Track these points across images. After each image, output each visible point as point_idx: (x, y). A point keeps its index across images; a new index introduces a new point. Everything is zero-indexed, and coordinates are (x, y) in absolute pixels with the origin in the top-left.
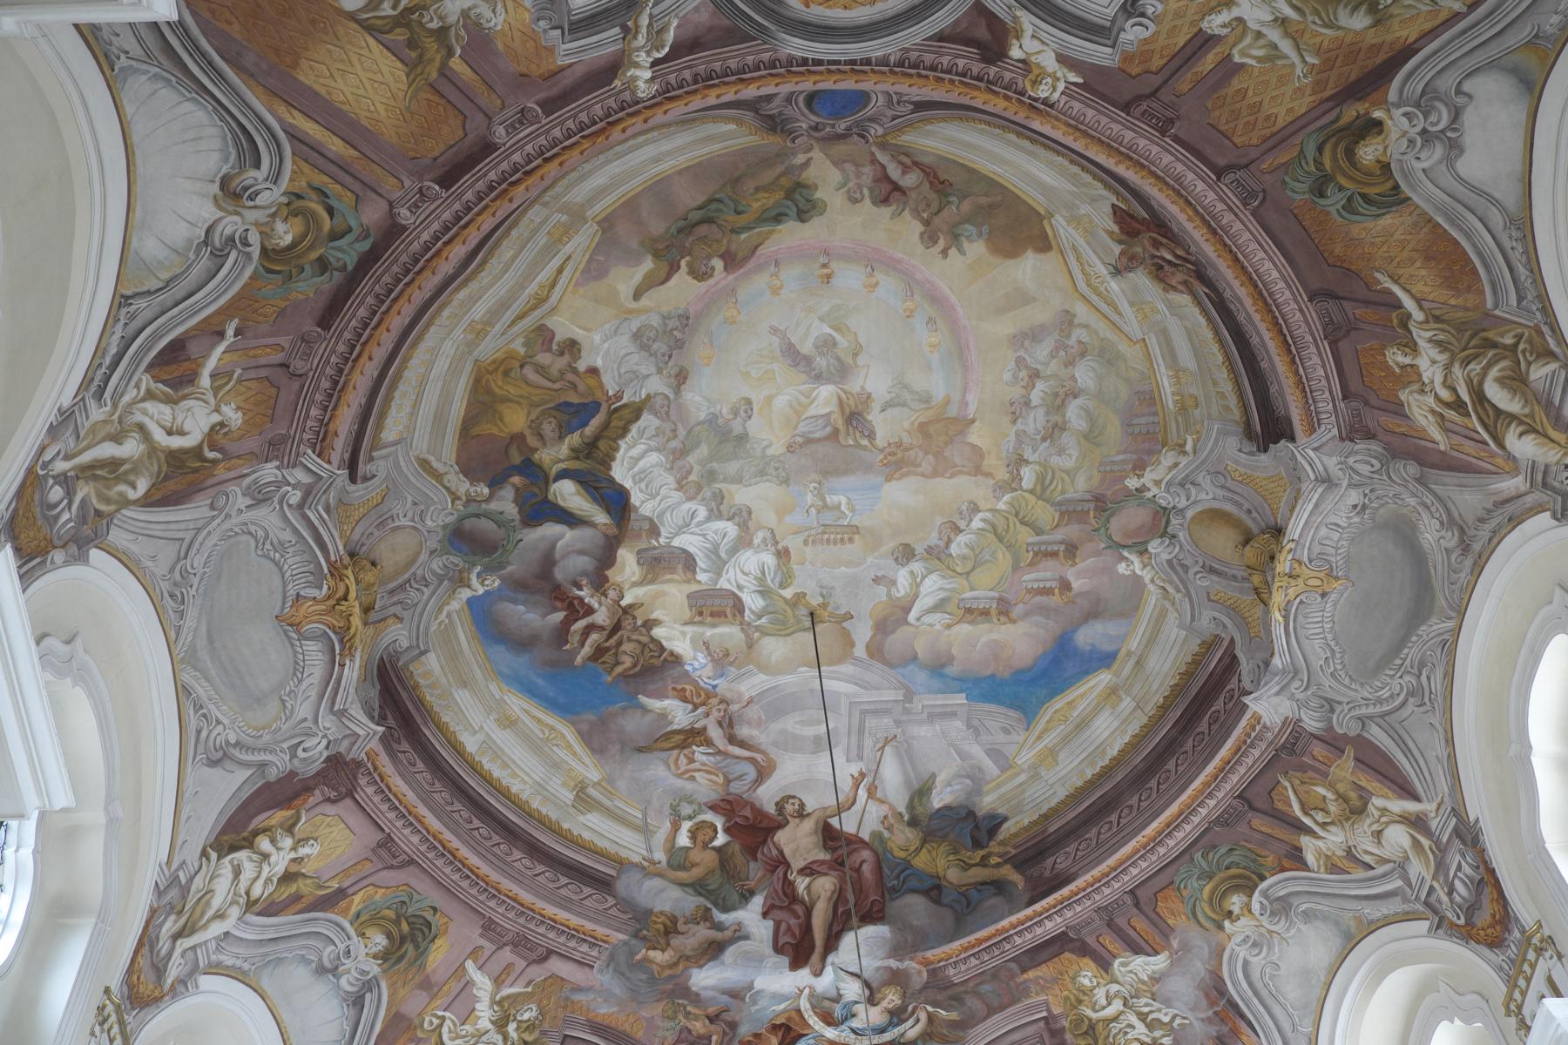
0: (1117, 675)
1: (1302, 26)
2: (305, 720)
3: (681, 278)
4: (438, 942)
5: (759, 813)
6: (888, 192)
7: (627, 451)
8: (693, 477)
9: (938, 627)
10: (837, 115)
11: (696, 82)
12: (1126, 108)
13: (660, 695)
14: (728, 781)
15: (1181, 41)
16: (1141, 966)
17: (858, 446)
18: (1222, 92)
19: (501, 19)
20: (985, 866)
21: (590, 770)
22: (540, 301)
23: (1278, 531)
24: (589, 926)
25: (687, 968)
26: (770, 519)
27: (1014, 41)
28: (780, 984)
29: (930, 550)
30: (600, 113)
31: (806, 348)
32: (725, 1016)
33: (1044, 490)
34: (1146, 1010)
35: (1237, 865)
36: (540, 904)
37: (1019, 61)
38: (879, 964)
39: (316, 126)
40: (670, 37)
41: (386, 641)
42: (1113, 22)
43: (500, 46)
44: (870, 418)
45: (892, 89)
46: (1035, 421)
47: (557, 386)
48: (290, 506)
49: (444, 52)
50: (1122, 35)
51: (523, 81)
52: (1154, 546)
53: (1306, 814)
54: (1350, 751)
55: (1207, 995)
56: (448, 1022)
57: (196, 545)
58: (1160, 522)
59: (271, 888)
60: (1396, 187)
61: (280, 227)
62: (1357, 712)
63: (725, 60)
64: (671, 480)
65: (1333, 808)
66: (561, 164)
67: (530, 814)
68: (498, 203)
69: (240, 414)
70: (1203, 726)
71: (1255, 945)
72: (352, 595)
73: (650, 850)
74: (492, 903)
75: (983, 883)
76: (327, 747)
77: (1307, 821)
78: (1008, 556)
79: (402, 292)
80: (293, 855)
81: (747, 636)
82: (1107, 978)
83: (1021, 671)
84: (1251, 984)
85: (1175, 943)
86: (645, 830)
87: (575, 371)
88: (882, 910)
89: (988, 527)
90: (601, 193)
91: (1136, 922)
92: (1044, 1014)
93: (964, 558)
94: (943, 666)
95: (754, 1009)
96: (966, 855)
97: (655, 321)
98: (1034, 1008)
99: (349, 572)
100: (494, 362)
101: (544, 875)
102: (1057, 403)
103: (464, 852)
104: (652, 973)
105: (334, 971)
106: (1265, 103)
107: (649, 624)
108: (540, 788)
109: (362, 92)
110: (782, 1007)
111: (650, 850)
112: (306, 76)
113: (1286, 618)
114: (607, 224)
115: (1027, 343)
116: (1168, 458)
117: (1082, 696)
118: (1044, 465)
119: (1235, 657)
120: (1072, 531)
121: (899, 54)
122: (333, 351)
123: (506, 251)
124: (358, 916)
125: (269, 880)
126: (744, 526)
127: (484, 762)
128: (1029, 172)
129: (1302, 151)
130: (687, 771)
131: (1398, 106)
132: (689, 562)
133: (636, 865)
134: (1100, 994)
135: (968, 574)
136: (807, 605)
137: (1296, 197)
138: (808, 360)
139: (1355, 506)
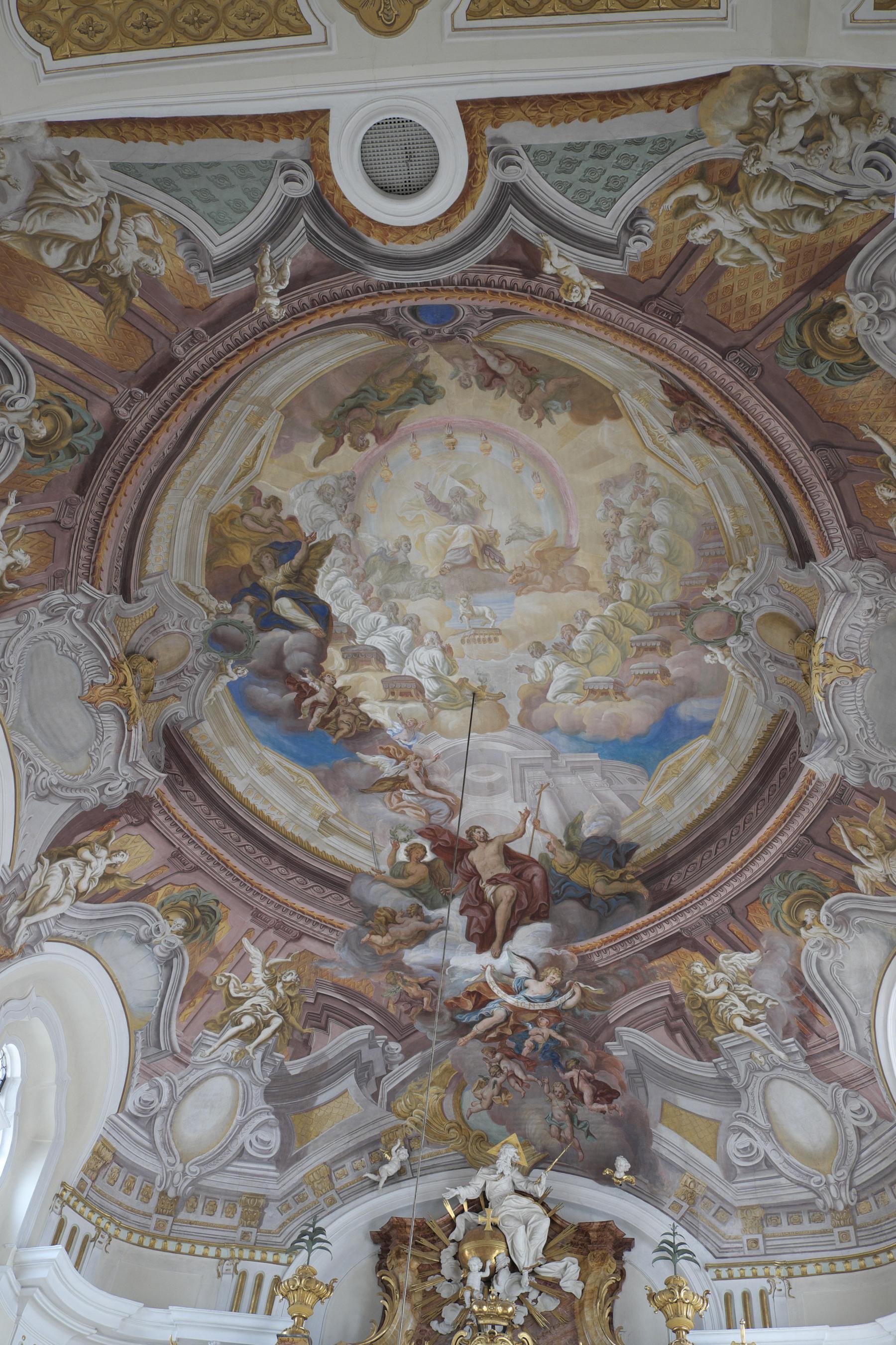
0: (714, 739)
1: (767, 233)
2: (108, 768)
3: (346, 449)
4: (222, 925)
5: (454, 838)
6: (490, 379)
7: (324, 576)
8: (374, 595)
9: (570, 703)
10: (440, 322)
11: (313, 306)
12: (641, 306)
13: (373, 753)
14: (429, 815)
15: (674, 251)
16: (740, 960)
17: (492, 570)
18: (715, 289)
19: (163, 267)
20: (622, 881)
21: (331, 807)
22: (247, 469)
23: (813, 630)
24: (328, 916)
25: (400, 949)
26: (434, 624)
27: (545, 260)
28: (469, 964)
29: (556, 646)
30: (249, 332)
31: (444, 498)
32: (432, 984)
33: (639, 600)
34: (745, 993)
35: (807, 887)
36: (291, 900)
37: (552, 275)
38: (542, 950)
39: (47, 352)
40: (288, 272)
41: (169, 713)
42: (619, 239)
43: (167, 287)
44: (498, 548)
45: (471, 303)
46: (626, 548)
47: (268, 530)
48: (77, 620)
49: (127, 294)
50: (628, 250)
51: (188, 311)
52: (731, 642)
53: (855, 849)
54: (882, 801)
55: (790, 984)
56: (233, 981)
57: (10, 648)
58: (734, 623)
59: (94, 885)
60: (866, 357)
61: (36, 424)
62: (887, 771)
63: (331, 287)
64: (358, 596)
65: (873, 845)
66: (227, 371)
67: (286, 836)
68: (187, 401)
69: (28, 557)
70: (775, 780)
71: (824, 948)
72: (130, 681)
73: (377, 863)
74: (257, 899)
75: (621, 894)
76: (127, 788)
77: (856, 854)
78: (618, 652)
79: (131, 467)
80: (108, 862)
81: (429, 710)
82: (715, 968)
83: (638, 737)
84: (823, 977)
85: (764, 944)
86: (373, 849)
87: (279, 519)
88: (547, 912)
89: (599, 629)
90: (280, 388)
91: (733, 927)
92: (668, 993)
93: (583, 652)
94: (578, 732)
95: (453, 980)
96: (609, 872)
97: (331, 481)
98: (661, 988)
99: (125, 666)
100: (222, 514)
101: (296, 879)
102: (642, 533)
103: (233, 862)
104: (373, 951)
105: (149, 942)
106: (749, 296)
107: (357, 701)
108: (293, 817)
109: (74, 325)
110: (473, 979)
111: (377, 863)
112: (32, 316)
113: (825, 697)
114: (287, 411)
115: (611, 489)
116: (734, 574)
117: (689, 755)
118: (637, 581)
119: (796, 727)
120: (664, 631)
121: (460, 276)
122: (90, 511)
123: (214, 434)
124: (162, 905)
125: (91, 879)
126: (415, 630)
127: (250, 798)
128: (596, 357)
129: (785, 332)
130: (399, 807)
131: (855, 292)
132: (380, 657)
133: (366, 874)
134: (710, 980)
135: (588, 664)
136: (470, 687)
137: (787, 368)
138: (447, 507)
139: (870, 611)
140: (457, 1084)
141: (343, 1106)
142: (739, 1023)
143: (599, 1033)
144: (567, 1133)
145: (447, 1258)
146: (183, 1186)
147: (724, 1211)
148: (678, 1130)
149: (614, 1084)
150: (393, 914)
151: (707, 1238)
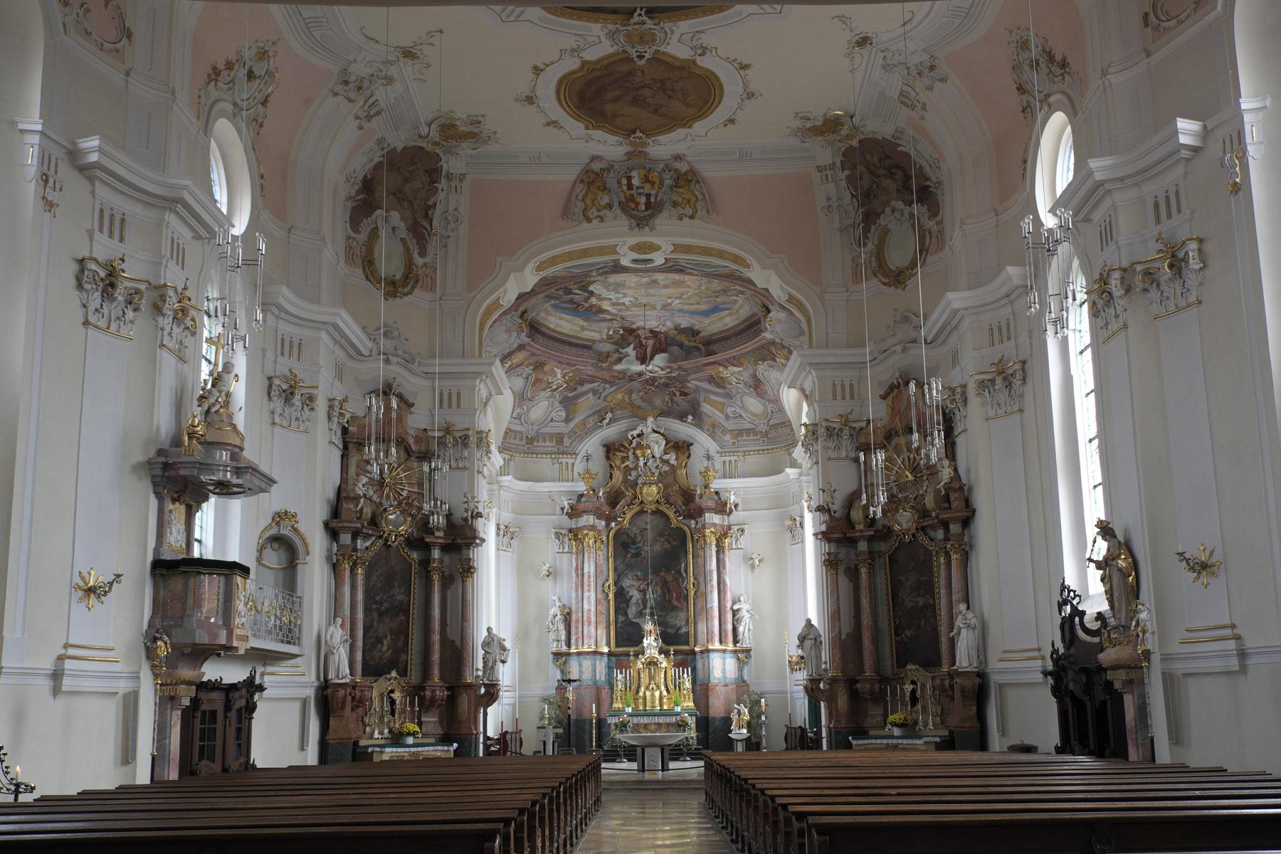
21: (585, 324)
86: (600, 332)
140: (630, 392)
141: (588, 403)
143: (682, 381)
145: (630, 454)
147: (725, 431)
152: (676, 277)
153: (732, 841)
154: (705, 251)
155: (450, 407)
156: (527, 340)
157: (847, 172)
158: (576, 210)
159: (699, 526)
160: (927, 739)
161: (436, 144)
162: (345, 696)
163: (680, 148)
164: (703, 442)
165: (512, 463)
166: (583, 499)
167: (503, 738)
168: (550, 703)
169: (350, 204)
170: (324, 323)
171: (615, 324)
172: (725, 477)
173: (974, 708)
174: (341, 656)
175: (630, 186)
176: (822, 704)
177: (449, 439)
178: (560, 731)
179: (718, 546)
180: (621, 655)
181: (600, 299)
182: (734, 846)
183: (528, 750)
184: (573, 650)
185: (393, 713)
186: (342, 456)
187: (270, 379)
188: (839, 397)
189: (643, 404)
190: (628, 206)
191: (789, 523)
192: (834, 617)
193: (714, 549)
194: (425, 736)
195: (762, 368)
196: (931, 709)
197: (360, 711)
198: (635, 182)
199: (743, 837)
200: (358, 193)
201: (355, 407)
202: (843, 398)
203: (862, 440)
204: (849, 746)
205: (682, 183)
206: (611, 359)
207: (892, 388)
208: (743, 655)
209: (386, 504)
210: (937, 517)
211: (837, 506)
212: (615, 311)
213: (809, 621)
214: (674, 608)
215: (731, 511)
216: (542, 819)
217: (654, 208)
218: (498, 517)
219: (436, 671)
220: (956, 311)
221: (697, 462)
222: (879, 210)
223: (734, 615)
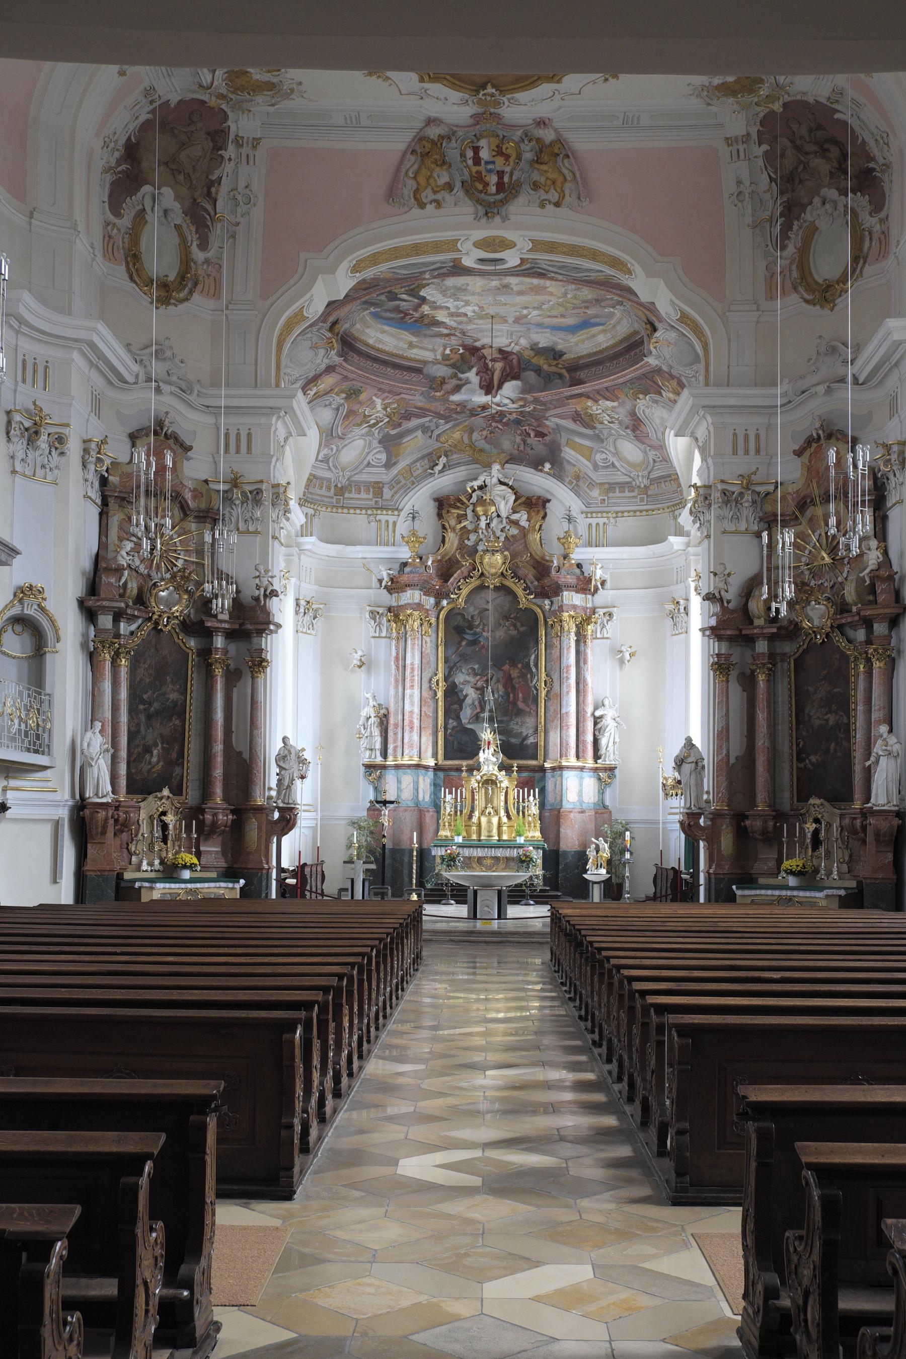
16: (609, 404)
21: (414, 339)
67: (393, 355)
91: (609, 394)
96: (551, 361)
134: (594, 408)
141: (415, 444)
142: (606, 422)
143: (539, 418)
144: (522, 448)
146: (343, 481)
147: (592, 485)
148: (574, 449)
149: (545, 431)
150: (444, 378)
151: (583, 498)
152: (536, 281)
153: (580, 1017)
154: (574, 251)
155: (238, 451)
156: (338, 360)
157: (765, 147)
158: (406, 192)
159: (555, 607)
160: (830, 892)
161: (222, 96)
162: (106, 819)
163: (543, 110)
164: (563, 498)
165: (316, 520)
166: (407, 569)
167: (300, 872)
168: (360, 828)
169: (109, 178)
170: (76, 340)
171: (454, 341)
172: (590, 545)
173: (890, 856)
174: (101, 771)
175: (477, 160)
176: (702, 844)
177: (237, 494)
178: (373, 866)
179: (578, 634)
180: (451, 769)
181: (434, 306)
182: (582, 1024)
183: (331, 887)
184: (390, 762)
185: (165, 840)
186: (101, 514)
187: (8, 413)
188: (741, 451)
189: (487, 447)
190: (473, 187)
191: (670, 607)
192: (722, 736)
193: (573, 637)
194: (204, 868)
195: (643, 405)
196: (837, 854)
197: (125, 836)
198: (484, 154)
199: (593, 1015)
200: (119, 162)
201: (117, 450)
202: (747, 452)
203: (768, 508)
204: (731, 898)
205: (545, 157)
206: (448, 387)
207: (809, 441)
208: (606, 774)
209: (156, 577)
210: (858, 613)
211: (732, 595)
212: (453, 324)
213: (689, 740)
214: (520, 713)
215: (596, 590)
216: (350, 993)
217: (507, 190)
218: (298, 589)
219: (218, 790)
220: (898, 344)
221: (555, 524)
222: (805, 201)
223: (595, 724)
